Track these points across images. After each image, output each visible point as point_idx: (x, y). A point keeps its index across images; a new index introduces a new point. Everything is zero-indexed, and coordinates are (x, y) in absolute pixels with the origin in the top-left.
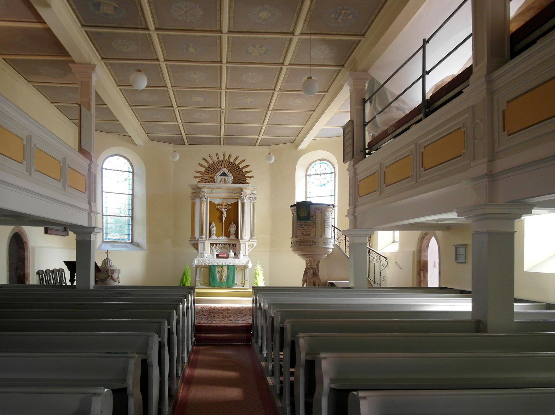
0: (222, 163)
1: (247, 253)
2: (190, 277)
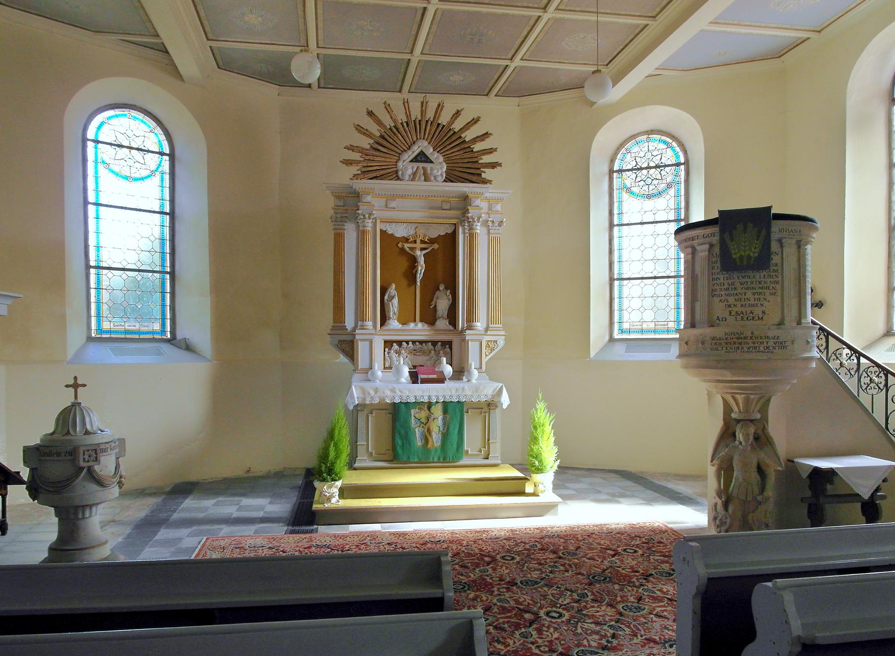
0: (418, 127)
1: (485, 360)
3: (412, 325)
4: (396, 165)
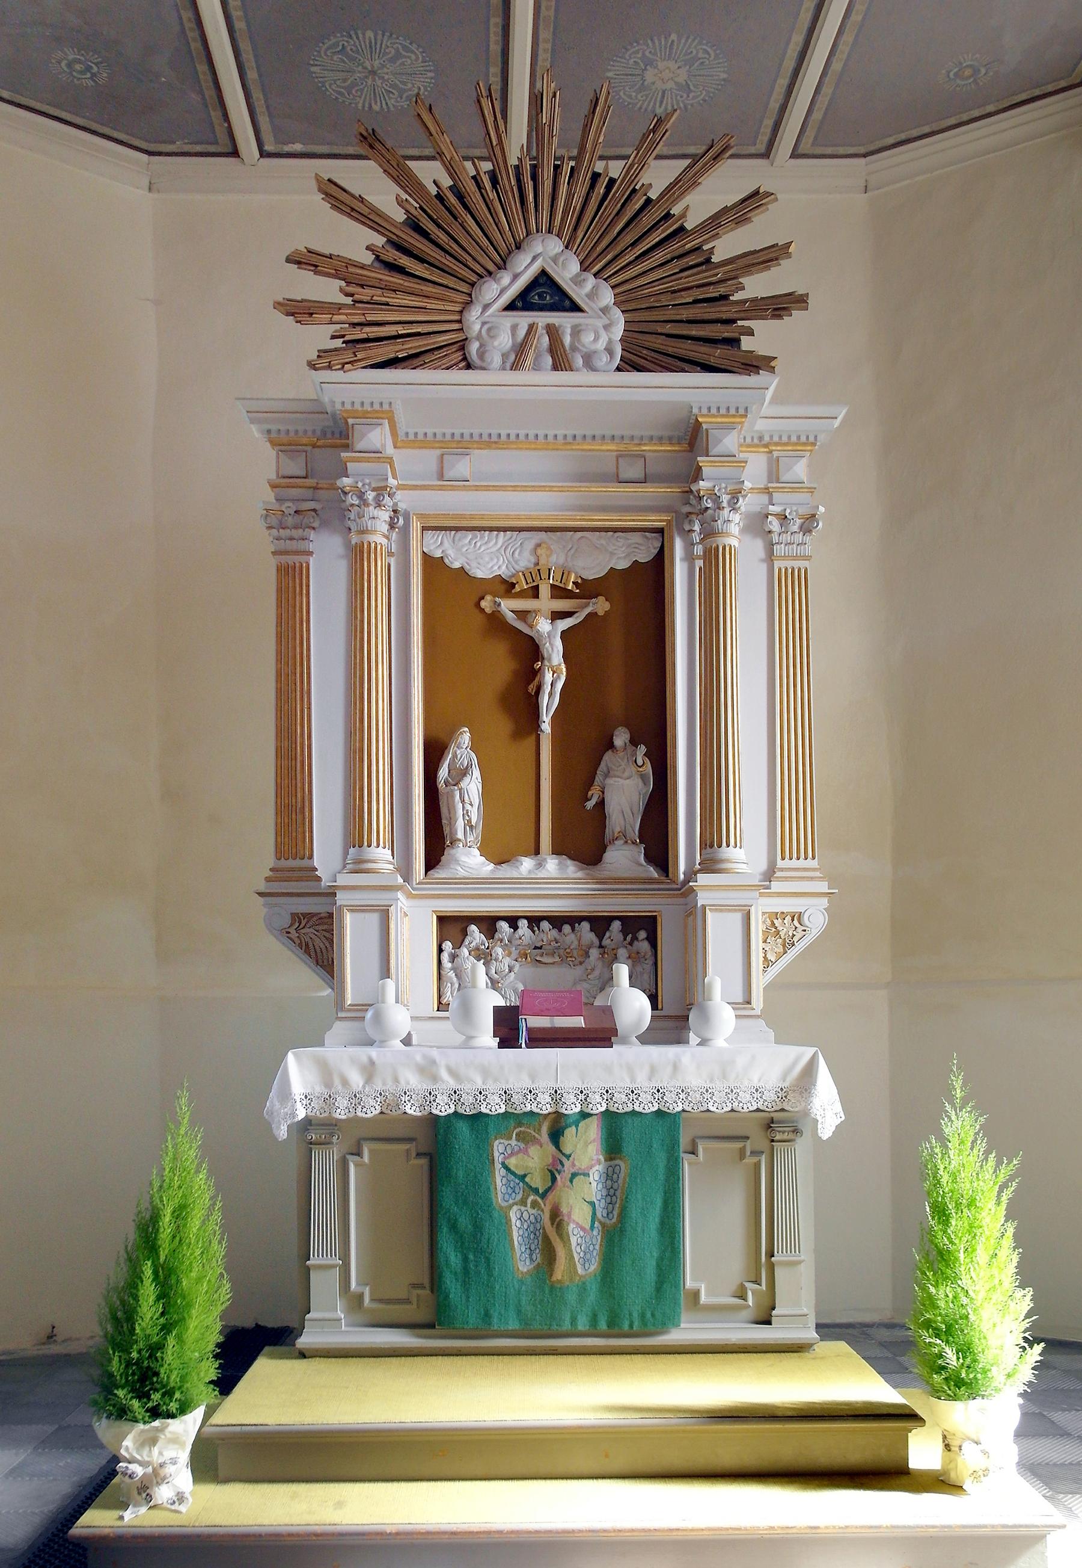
1: (760, 981)
2: (216, 1268)
3: (527, 864)
4: (460, 321)
